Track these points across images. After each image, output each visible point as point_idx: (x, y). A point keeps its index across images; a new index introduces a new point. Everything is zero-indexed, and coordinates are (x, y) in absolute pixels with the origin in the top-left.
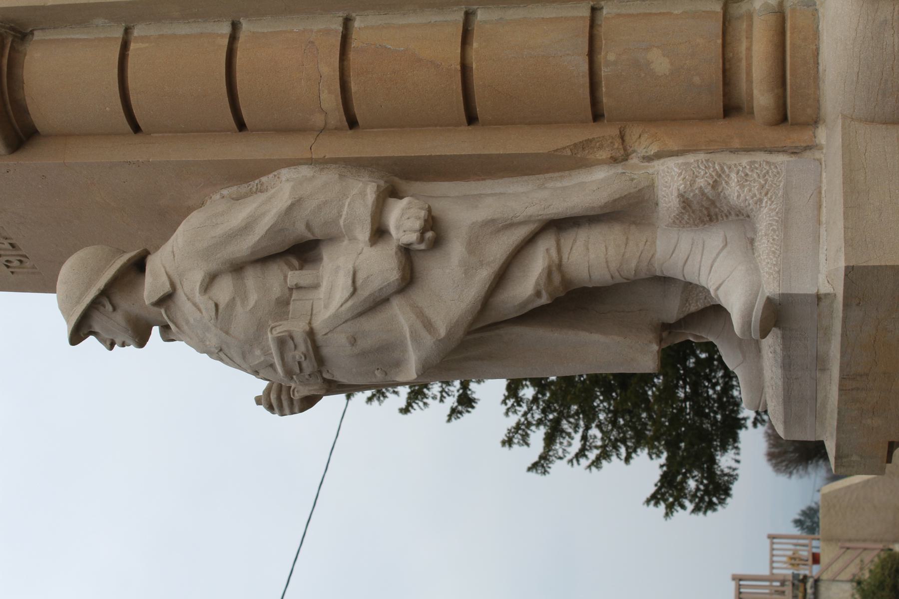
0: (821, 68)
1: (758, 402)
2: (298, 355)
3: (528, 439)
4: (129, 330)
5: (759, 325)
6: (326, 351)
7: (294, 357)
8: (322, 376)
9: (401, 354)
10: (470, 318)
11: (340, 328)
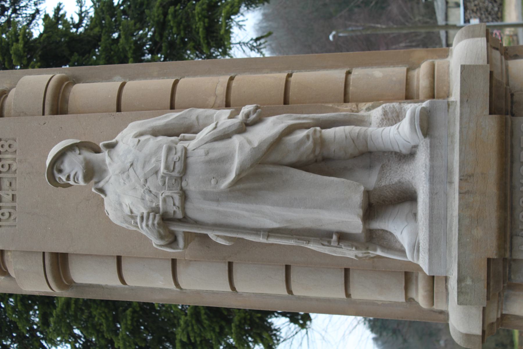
0: (450, 70)
1: (414, 241)
2: (176, 157)
3: (274, 325)
4: (83, 163)
5: (419, 114)
6: (190, 160)
7: (173, 158)
8: (181, 185)
9: (230, 166)
10: (271, 140)
11: (202, 146)
